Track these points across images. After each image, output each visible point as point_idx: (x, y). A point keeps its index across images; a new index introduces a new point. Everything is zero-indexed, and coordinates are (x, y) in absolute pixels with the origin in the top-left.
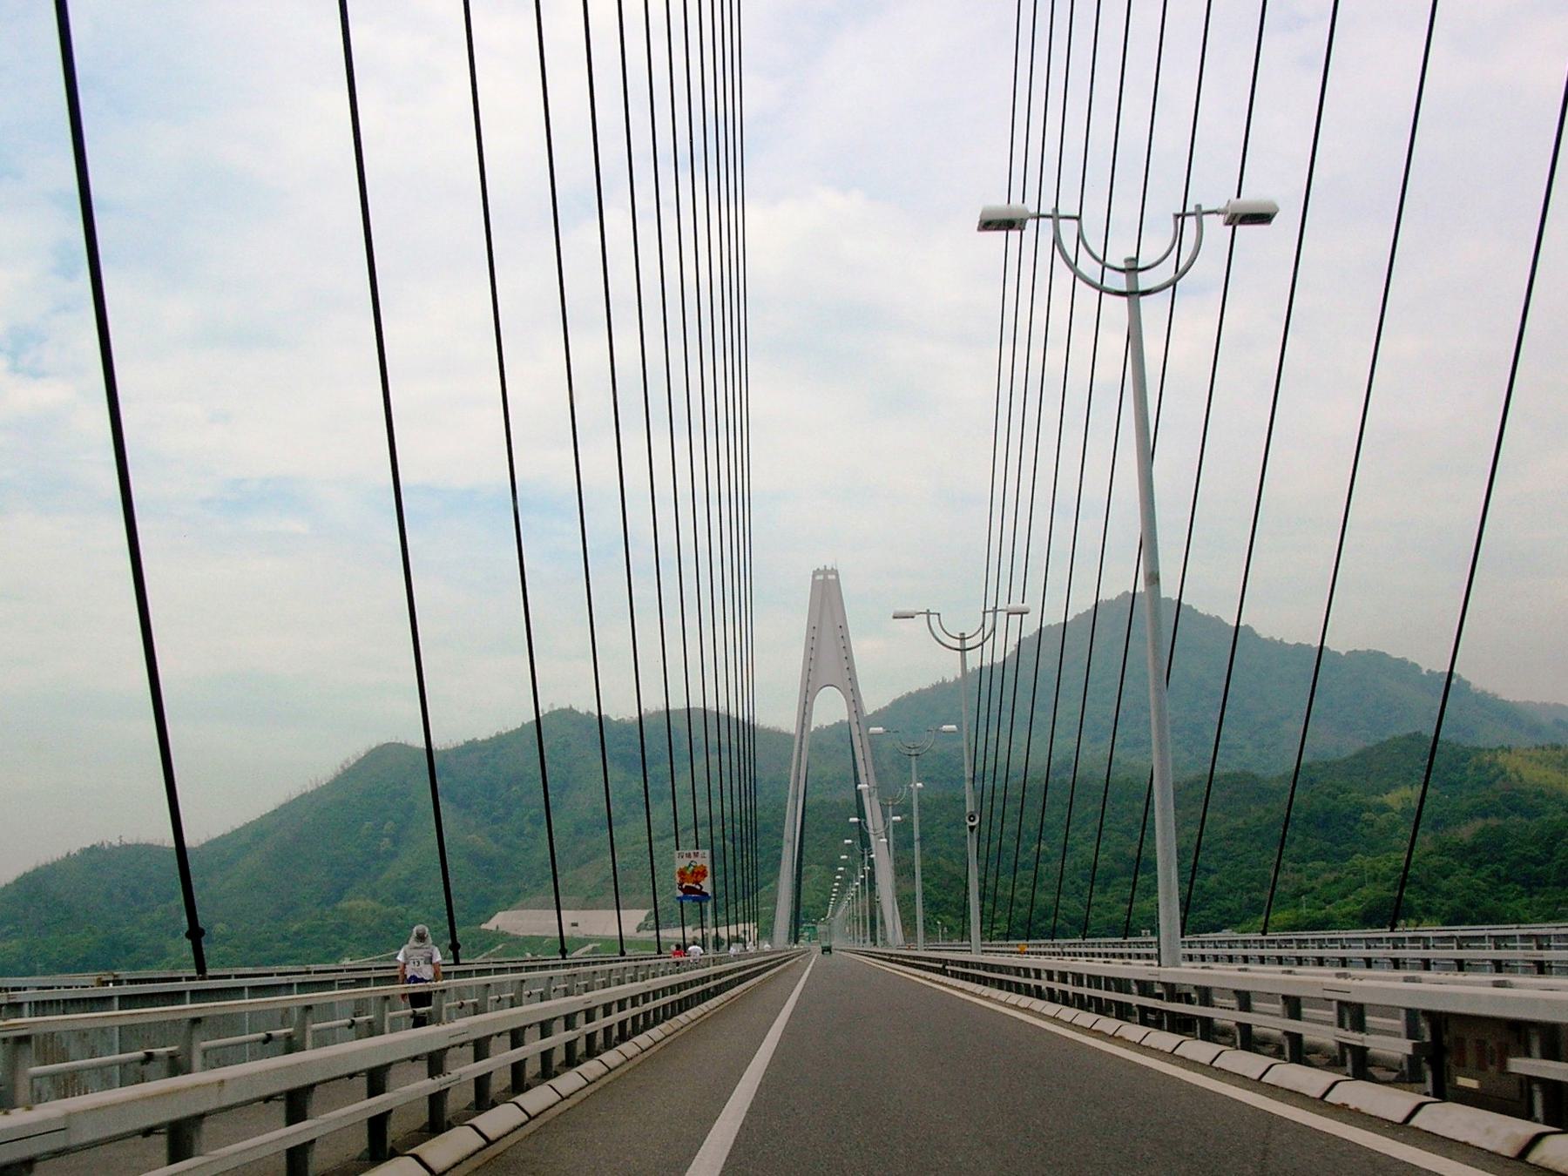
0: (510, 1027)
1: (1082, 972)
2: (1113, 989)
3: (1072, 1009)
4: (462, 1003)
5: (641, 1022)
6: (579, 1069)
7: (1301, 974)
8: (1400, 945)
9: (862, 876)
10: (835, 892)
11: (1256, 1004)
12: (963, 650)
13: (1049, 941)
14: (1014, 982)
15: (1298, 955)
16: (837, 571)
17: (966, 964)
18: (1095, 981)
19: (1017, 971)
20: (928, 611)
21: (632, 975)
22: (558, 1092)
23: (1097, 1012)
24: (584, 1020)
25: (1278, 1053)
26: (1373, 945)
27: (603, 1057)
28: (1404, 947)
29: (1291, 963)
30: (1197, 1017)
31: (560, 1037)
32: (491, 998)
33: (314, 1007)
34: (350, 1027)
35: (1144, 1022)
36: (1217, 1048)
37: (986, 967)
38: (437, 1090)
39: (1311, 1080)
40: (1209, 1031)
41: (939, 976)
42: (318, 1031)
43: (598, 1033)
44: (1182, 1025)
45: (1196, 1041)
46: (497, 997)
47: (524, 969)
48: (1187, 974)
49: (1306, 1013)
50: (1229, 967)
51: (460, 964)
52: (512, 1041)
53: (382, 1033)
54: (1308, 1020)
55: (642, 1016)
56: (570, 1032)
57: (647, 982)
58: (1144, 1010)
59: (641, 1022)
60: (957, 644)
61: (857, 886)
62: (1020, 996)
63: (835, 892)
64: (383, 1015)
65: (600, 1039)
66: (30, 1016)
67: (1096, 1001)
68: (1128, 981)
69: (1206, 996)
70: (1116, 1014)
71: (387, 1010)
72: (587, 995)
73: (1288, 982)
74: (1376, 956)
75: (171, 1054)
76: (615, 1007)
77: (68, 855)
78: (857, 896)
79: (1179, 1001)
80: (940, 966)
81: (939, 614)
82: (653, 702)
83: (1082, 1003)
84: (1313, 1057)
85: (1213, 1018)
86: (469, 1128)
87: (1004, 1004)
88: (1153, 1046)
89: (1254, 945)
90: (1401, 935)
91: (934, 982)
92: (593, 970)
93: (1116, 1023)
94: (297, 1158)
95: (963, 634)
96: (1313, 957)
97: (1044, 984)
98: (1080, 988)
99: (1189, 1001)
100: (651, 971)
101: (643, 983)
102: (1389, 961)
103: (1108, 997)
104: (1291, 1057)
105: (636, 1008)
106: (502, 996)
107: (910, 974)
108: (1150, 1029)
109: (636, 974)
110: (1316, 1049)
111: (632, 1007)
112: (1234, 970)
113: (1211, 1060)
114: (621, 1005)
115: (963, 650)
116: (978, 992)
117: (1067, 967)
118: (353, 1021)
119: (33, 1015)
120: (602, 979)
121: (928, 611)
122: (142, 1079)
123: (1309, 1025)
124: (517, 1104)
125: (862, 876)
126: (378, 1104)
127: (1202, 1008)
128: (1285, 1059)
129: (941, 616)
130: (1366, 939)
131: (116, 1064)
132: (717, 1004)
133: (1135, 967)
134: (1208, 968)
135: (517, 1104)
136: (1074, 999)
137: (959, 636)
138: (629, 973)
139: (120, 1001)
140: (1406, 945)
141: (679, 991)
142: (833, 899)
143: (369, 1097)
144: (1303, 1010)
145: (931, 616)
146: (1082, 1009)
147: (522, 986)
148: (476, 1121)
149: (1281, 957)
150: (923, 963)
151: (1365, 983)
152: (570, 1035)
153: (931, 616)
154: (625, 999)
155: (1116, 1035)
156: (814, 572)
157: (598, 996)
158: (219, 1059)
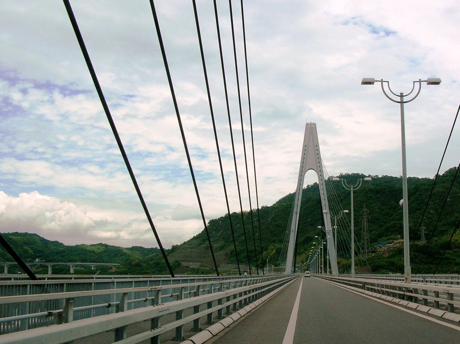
0: (194, 306)
1: (375, 283)
2: (398, 290)
3: (380, 294)
4: (215, 288)
5: (251, 299)
6: (238, 312)
7: (453, 287)
8: (453, 278)
9: (318, 253)
10: (309, 258)
11: (429, 293)
12: (402, 103)
13: (432, 275)
14: (398, 293)
15: (446, 281)
16: (315, 124)
17: (350, 281)
18: (387, 287)
19: (378, 285)
20: (382, 80)
21: (249, 282)
22: (240, 315)
23: (387, 295)
24: (239, 296)
25: (447, 309)
26: (447, 278)
27: (239, 311)
28: (454, 279)
29: (438, 283)
30: (413, 296)
31: (214, 309)
32: (201, 290)
33: (128, 293)
34: (171, 297)
35: (399, 298)
36: (429, 308)
37: (356, 282)
38: (153, 336)
39: (439, 312)
40: (416, 300)
41: (342, 284)
42: (129, 303)
43: (237, 303)
44: (410, 299)
45: (422, 305)
46: (203, 290)
47: (242, 278)
48: (412, 285)
49: (440, 296)
50: (422, 283)
51: (175, 277)
52: (227, 299)
53: (67, 321)
54: (455, 300)
55: (251, 297)
56: (220, 306)
57: (250, 286)
58: (400, 294)
59: (251, 299)
60: (398, 99)
61: (316, 256)
62: (369, 291)
63: (309, 258)
64: (182, 293)
65: (243, 302)
66: (66, 292)
67: (399, 295)
68: (396, 286)
69: (416, 291)
70: (387, 294)
71: (213, 287)
72: (227, 291)
73: (386, 283)
74: (442, 281)
75: (153, 299)
76: (243, 294)
77: (184, 242)
78: (316, 259)
79: (409, 292)
80: (331, 279)
81: (388, 82)
82: (254, 207)
83: (388, 294)
84: (457, 311)
85: (418, 297)
86: (230, 318)
87: (367, 295)
88: (421, 310)
89: (433, 278)
90: (436, 276)
91: (347, 288)
92: (241, 280)
93: (407, 302)
94: (154, 340)
95: (402, 94)
96: (455, 282)
97: (376, 288)
98: (383, 289)
99: (412, 292)
100: (243, 283)
101: (249, 286)
102: (456, 283)
103: (390, 291)
104: (436, 307)
105: (246, 295)
106: (216, 288)
107: (335, 284)
108: (401, 300)
109: (250, 282)
110: (443, 305)
111: (245, 295)
112: (445, 286)
113: (442, 315)
114: (235, 296)
115: (402, 103)
116: (355, 290)
117: (379, 283)
118: (172, 295)
119: (34, 293)
120: (218, 287)
121: (382, 80)
122: (108, 313)
123: (456, 302)
124: (192, 341)
125: (318, 253)
126: (156, 332)
127: (425, 296)
128: (434, 308)
129: (389, 82)
130: (431, 276)
131: (16, 320)
132: (272, 295)
133: (420, 285)
134: (437, 285)
135: (192, 341)
136: (385, 293)
137: (400, 95)
138: (248, 282)
139: (172, 281)
140: (454, 278)
141: (261, 289)
142: (309, 260)
143: (208, 308)
144: (454, 297)
145: (384, 83)
146: (388, 295)
147: (212, 286)
148: (191, 338)
149: (446, 282)
150: (336, 280)
151: (453, 288)
152: (220, 307)
153: (384, 83)
154: (242, 292)
155: (392, 301)
156: (306, 124)
157: (232, 291)
158: (78, 316)
